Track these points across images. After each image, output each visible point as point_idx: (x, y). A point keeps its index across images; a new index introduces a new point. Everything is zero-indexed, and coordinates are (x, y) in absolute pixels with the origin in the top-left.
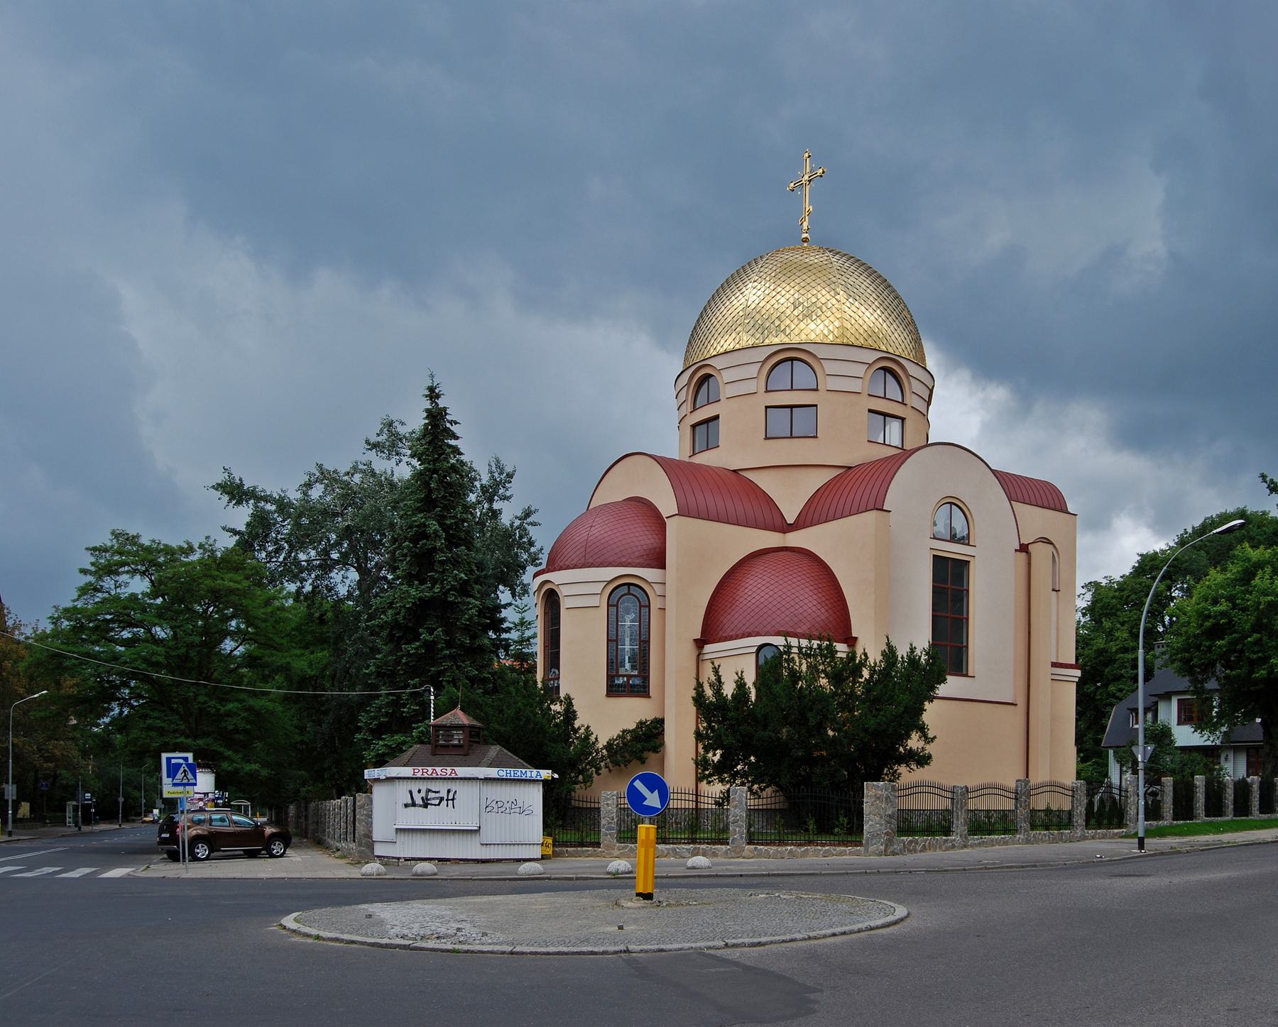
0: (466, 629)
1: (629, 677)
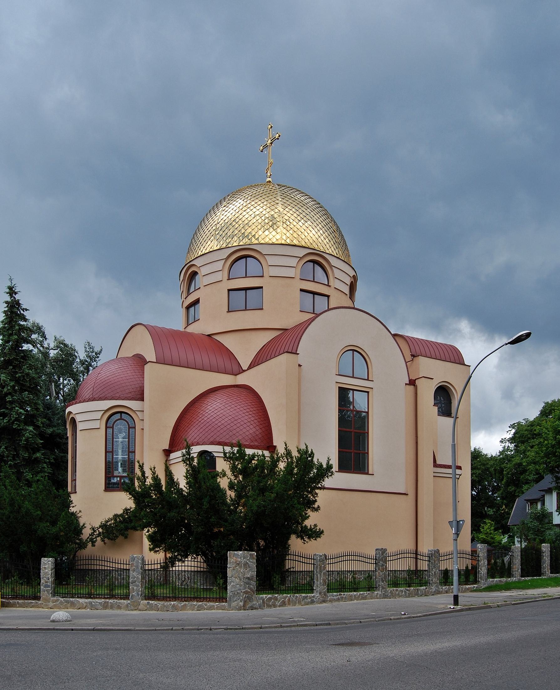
0: (25, 448)
1: (121, 477)
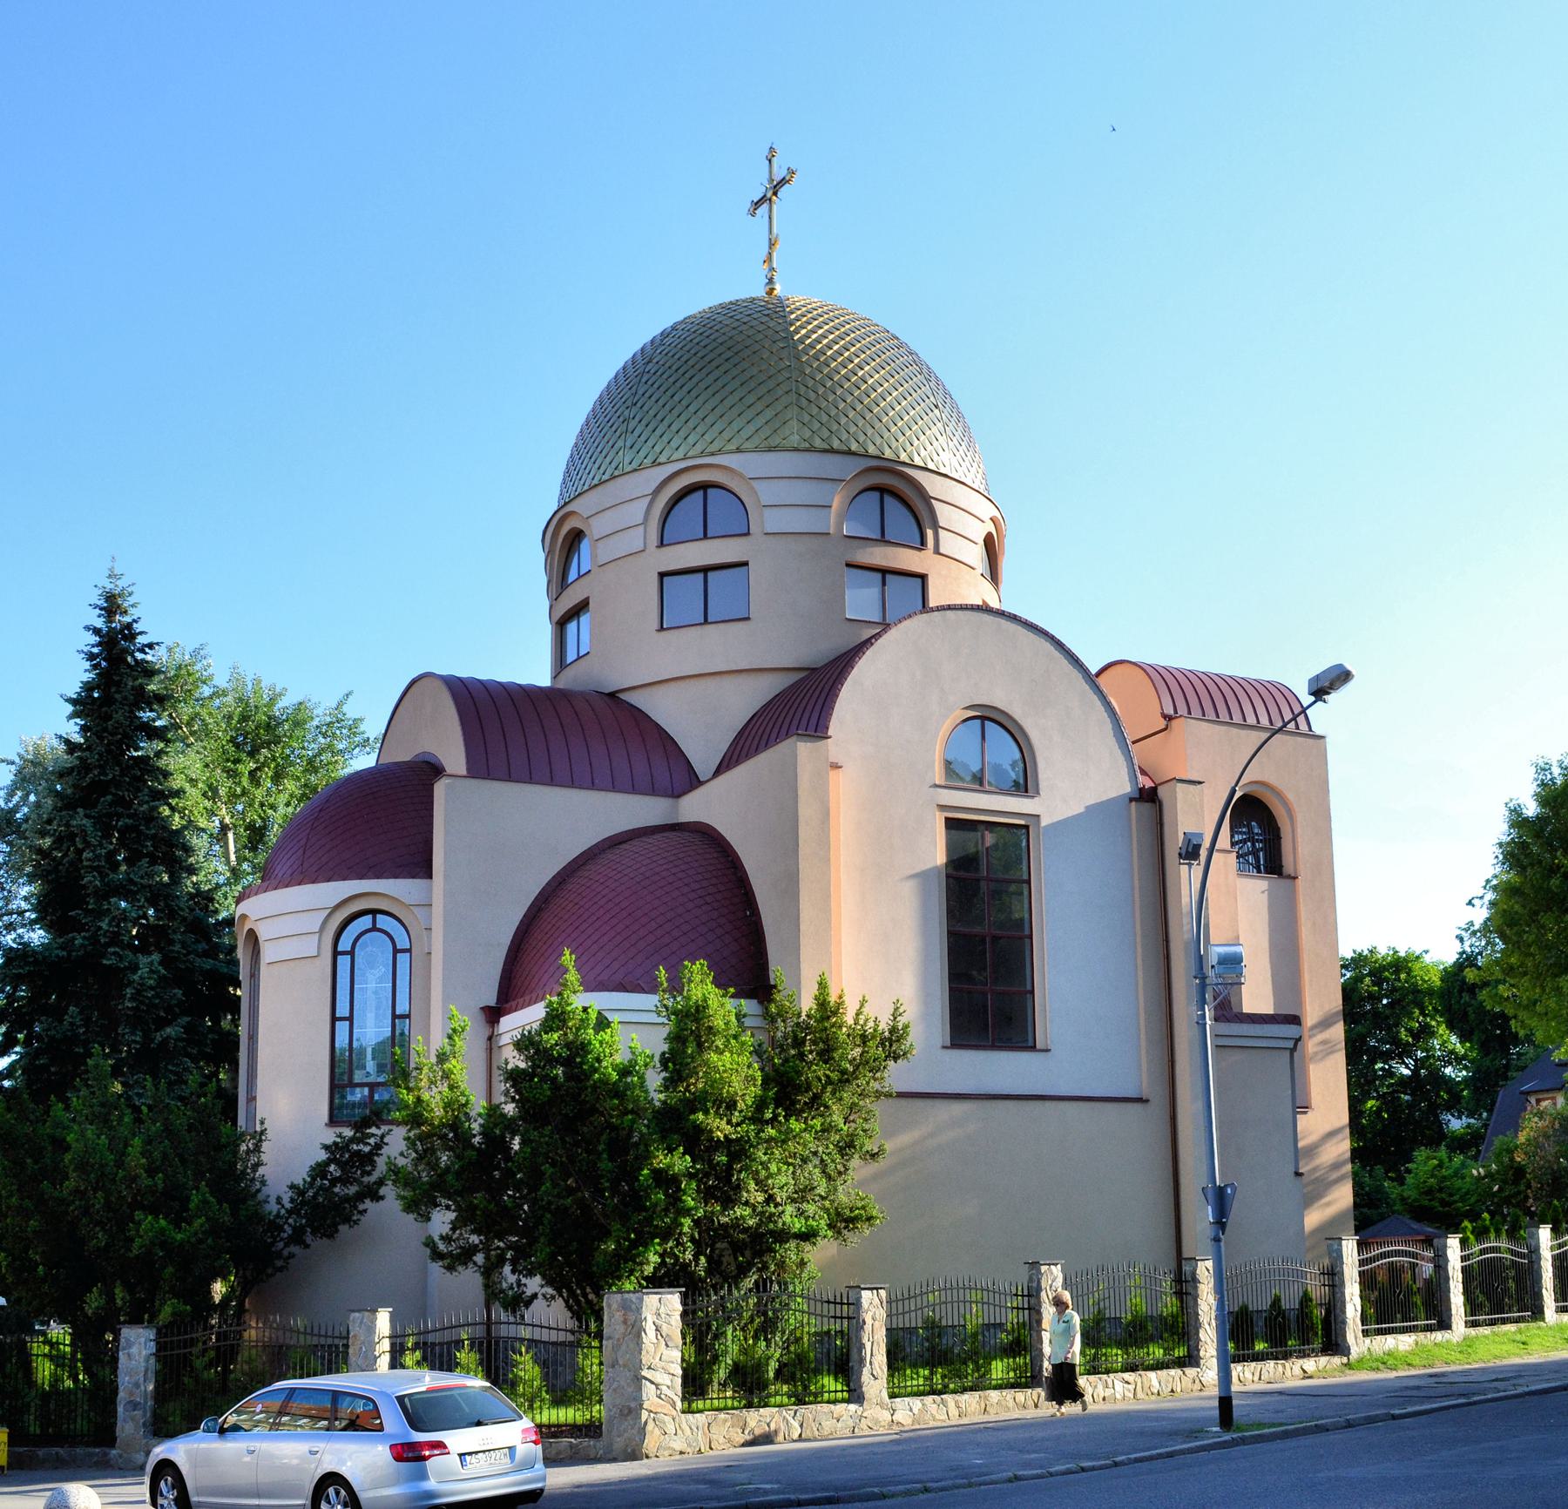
1: (372, 1087)
